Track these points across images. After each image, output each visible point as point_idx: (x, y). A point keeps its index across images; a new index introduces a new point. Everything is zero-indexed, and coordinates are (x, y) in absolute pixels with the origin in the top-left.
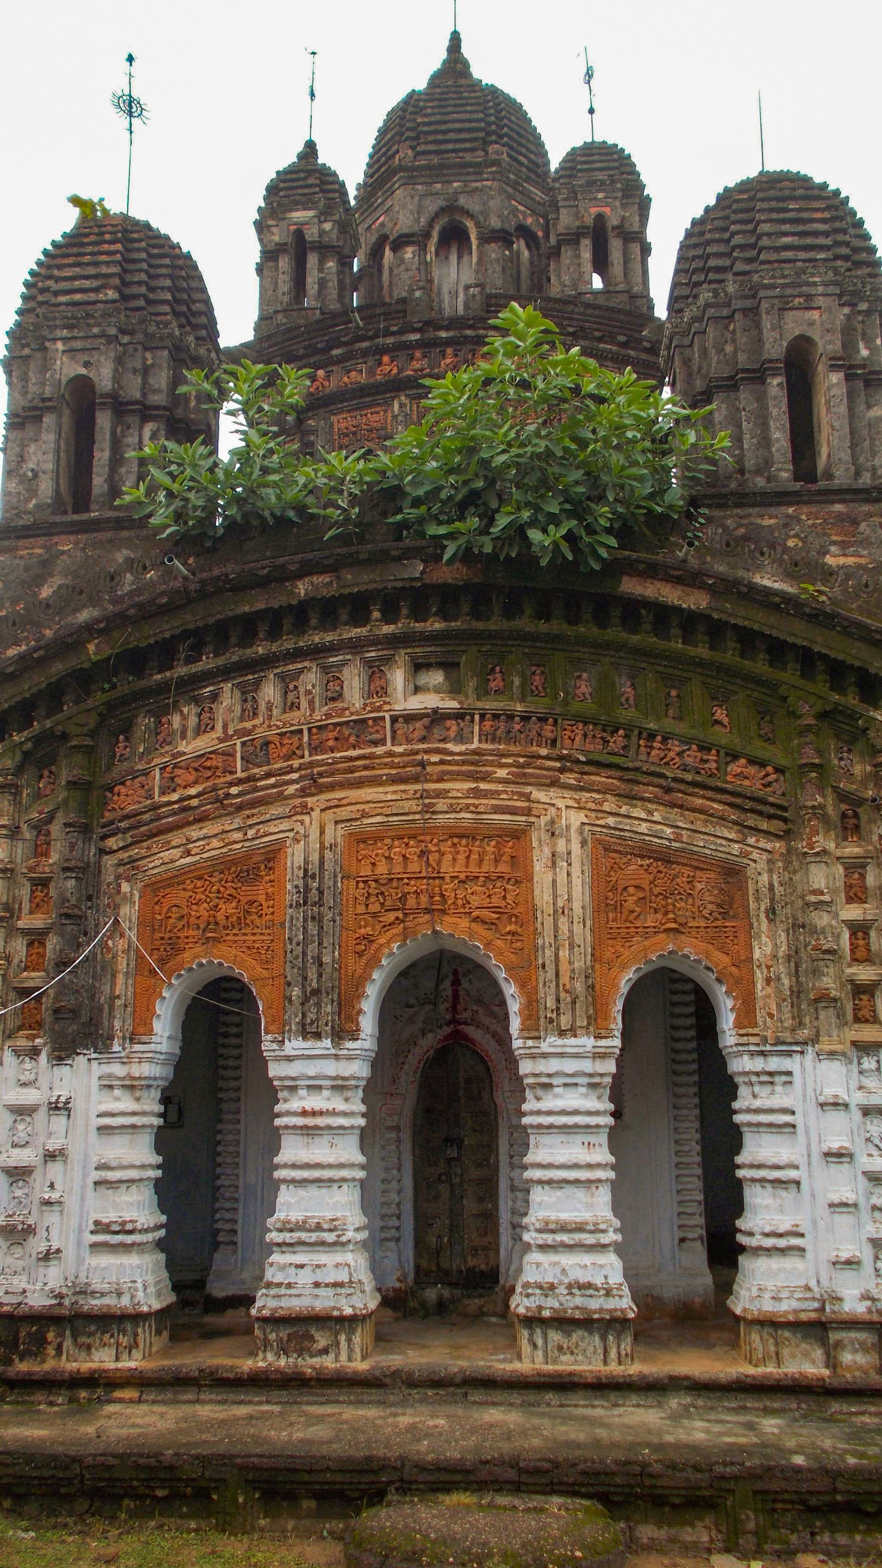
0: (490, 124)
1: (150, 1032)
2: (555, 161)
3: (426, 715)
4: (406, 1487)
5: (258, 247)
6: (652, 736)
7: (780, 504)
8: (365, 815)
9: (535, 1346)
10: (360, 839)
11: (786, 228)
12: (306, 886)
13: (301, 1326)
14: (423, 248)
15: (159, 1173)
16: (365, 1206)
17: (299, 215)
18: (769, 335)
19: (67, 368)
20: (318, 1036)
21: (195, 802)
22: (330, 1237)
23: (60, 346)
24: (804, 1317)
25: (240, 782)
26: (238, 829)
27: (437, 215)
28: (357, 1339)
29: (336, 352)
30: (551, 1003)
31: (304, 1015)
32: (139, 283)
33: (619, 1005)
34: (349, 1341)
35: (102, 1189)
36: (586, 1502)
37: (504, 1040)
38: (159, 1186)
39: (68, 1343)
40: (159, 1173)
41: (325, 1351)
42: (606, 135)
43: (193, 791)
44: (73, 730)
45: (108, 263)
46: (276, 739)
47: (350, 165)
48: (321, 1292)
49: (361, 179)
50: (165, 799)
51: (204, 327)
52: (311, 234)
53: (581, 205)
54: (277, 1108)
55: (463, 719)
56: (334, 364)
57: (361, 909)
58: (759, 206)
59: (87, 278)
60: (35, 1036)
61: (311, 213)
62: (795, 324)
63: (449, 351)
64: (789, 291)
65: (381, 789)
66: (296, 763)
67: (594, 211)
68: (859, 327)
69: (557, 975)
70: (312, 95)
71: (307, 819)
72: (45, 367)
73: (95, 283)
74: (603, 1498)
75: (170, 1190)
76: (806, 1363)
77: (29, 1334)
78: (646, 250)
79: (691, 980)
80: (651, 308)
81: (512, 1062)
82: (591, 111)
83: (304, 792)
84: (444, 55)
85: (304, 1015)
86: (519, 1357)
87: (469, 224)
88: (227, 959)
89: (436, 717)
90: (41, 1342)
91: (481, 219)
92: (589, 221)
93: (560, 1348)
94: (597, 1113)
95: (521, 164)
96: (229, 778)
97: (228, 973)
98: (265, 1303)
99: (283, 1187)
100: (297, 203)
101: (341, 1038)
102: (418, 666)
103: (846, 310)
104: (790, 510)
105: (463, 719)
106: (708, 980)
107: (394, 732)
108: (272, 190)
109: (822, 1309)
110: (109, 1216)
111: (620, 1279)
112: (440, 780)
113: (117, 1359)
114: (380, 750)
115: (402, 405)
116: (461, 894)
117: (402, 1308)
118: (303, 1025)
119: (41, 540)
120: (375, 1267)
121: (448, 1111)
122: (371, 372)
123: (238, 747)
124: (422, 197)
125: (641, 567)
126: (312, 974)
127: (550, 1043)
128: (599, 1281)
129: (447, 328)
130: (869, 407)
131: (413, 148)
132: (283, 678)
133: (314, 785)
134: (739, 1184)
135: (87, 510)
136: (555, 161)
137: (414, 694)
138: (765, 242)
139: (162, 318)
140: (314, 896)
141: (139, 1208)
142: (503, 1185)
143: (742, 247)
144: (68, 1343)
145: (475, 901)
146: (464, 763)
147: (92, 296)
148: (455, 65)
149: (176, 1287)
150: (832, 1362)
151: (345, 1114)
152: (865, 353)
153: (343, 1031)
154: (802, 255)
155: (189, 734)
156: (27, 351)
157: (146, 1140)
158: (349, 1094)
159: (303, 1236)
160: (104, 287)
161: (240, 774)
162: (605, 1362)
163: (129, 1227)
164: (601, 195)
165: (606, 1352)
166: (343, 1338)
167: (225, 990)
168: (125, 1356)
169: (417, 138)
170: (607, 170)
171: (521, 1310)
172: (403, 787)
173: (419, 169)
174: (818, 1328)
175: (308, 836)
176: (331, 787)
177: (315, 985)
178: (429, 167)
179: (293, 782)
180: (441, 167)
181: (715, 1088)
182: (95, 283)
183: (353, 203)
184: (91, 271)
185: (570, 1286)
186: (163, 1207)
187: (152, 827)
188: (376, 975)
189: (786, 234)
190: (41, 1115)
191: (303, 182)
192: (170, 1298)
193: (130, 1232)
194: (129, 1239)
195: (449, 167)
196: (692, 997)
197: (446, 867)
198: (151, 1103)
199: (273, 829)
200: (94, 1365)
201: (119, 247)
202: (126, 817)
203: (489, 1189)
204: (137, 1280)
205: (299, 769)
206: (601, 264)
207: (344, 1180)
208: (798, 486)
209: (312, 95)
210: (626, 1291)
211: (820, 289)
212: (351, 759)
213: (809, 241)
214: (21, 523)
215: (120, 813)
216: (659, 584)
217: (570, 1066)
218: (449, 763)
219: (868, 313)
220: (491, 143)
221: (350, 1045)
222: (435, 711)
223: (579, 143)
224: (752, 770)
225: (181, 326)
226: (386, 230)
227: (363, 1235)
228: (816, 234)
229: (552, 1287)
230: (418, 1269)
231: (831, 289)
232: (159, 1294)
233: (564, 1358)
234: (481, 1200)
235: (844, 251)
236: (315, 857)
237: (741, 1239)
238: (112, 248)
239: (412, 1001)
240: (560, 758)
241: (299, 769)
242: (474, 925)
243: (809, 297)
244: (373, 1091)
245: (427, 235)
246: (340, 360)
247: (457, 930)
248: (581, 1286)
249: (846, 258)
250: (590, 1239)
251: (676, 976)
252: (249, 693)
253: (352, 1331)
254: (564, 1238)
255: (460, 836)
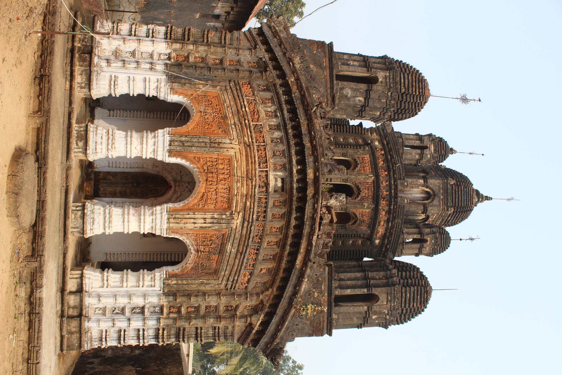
0: (460, 208)
1: (174, 94)
2: (448, 229)
3: (267, 181)
4: (40, 168)
5: (424, 134)
6: (258, 250)
7: (328, 291)
8: (237, 161)
9: (77, 207)
10: (230, 160)
11: (412, 295)
12: (216, 143)
13: (84, 138)
14: (423, 186)
15: (131, 95)
16: (119, 158)
17: (432, 148)
18: (379, 289)
19: (381, 75)
20: (170, 145)
21: (244, 109)
22: (110, 147)
23: (388, 74)
24: (84, 286)
25: (249, 124)
26: (235, 123)
27: (433, 191)
28: (80, 154)
29: (389, 157)
30: (177, 216)
31: (176, 141)
32: (406, 99)
33: (176, 237)
34: (80, 152)
35: (128, 79)
36: (34, 219)
37: (167, 202)
38: (128, 95)
39: (83, 68)
40: (131, 95)
41: (77, 144)
42: (452, 243)
43: (247, 109)
44: (268, 73)
45: (412, 90)
46: (262, 135)
47: (449, 163)
48: (94, 144)
49: (447, 167)
50: (245, 100)
51: (394, 118)
52: (427, 152)
53: (431, 235)
54: (149, 132)
55: (266, 192)
56: (386, 157)
57: (208, 159)
58: (419, 288)
59: (408, 83)
60: (174, 59)
61: (433, 151)
62: (383, 298)
63: (388, 193)
64: (392, 295)
65: (245, 166)
66: (254, 141)
67: (429, 239)
68: (381, 316)
69: (186, 218)
70: (471, 154)
71: (237, 143)
72: (381, 69)
73: (406, 86)
74: (34, 225)
75: (126, 97)
76: (72, 285)
77: (86, 57)
78: (417, 255)
79: (182, 260)
80: (398, 256)
81: (160, 204)
82: (461, 240)
83: (245, 143)
84: (485, 195)
85: (176, 141)
86: (73, 202)
87: (430, 201)
88: (195, 118)
89: (267, 185)
90: (84, 60)
91: (431, 204)
92: (426, 237)
93: (76, 214)
94: (144, 229)
95: (448, 217)
96: (251, 120)
97: (191, 116)
98: (91, 127)
99: (125, 133)
100: (436, 147)
101: (169, 152)
102: (283, 180)
103: (386, 312)
104: (326, 294)
105: (266, 192)
106: (183, 264)
107: (263, 171)
108: (441, 140)
109: (86, 292)
110: (119, 81)
111: (96, 233)
112: (247, 185)
113: (78, 83)
114: (257, 166)
115: (371, 177)
116: (212, 190)
117: (88, 167)
118: (173, 141)
119: (328, 65)
120: (101, 160)
121: (145, 184)
122: (382, 168)
123: (260, 123)
124: (439, 186)
125: (309, 248)
126: (189, 144)
127: (165, 216)
128: (95, 226)
129: (395, 192)
130: (357, 318)
131: (454, 184)
132: (281, 139)
133: (248, 146)
134: (122, 270)
135: (336, 80)
136: (448, 229)
137: (275, 179)
138: (408, 289)
139: (396, 105)
140: (213, 145)
141: (121, 90)
142: (124, 199)
143: (408, 282)
144: (83, 68)
145: (209, 194)
146: (252, 192)
147: (402, 85)
148: (481, 198)
149: (98, 100)
150: (71, 293)
151: (147, 152)
152: (374, 317)
153: (171, 153)
154: (403, 300)
155: (265, 109)
156: (387, 64)
157: (141, 92)
158: (152, 153)
159: (111, 139)
160: (405, 88)
161: (252, 123)
162: (72, 228)
163: (116, 87)
164: (433, 241)
165: (75, 228)
166: (81, 150)
167: (185, 115)
168: (78, 85)
169: (457, 185)
170: (442, 243)
171: (87, 203)
172: (245, 173)
173: (447, 185)
174: (80, 290)
175: (233, 148)
176: (246, 151)
177: (186, 144)
178: (447, 189)
179: (249, 140)
180: (447, 193)
181: (151, 265)
182: (406, 86)
183: (440, 164)
184: (410, 86)
185: (93, 218)
186: (122, 96)
187: (238, 96)
188: (188, 163)
189: (410, 295)
190: (150, 60)
191: (443, 148)
192: (94, 99)
193: (114, 86)
194: (112, 87)
195: (447, 195)
196: (177, 260)
197: (220, 186)
198: (153, 93)
199: (234, 133)
200: (76, 76)
201: (417, 94)
202: (240, 89)
203: (123, 195)
204: (100, 90)
205: (252, 142)
206: (415, 241)
207: (127, 151)
208: (333, 297)
209: (471, 154)
210: (92, 235)
211: (393, 304)
212: (255, 158)
213: (407, 301)
214: (334, 60)
215: (241, 86)
216: (304, 254)
217: (158, 221)
218: (252, 188)
219: (386, 319)
220: (454, 209)
221: (167, 154)
222: (269, 184)
223: (450, 235)
224: (246, 279)
225: (394, 111)
226: (430, 174)
227: (110, 157)
228: (409, 304)
229: (93, 213)
230: (100, 172)
231: (392, 308)
232: (96, 95)
233: (73, 215)
234: (120, 192)
235: (404, 312)
236: (225, 146)
237: (106, 270)
238: (417, 92)
239: (182, 173)
240: (252, 222)
241: (252, 142)
242: (202, 193)
243: (391, 301)
244: (154, 162)
245: (427, 187)
246: (387, 158)
247: (201, 188)
248: (93, 221)
249: (402, 313)
250: (107, 225)
251: (184, 255)
252: (278, 128)
253: (83, 153)
254: (108, 216)
255: (229, 190)
